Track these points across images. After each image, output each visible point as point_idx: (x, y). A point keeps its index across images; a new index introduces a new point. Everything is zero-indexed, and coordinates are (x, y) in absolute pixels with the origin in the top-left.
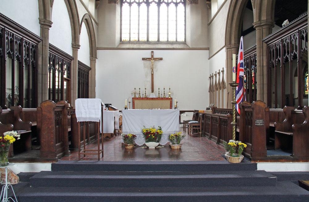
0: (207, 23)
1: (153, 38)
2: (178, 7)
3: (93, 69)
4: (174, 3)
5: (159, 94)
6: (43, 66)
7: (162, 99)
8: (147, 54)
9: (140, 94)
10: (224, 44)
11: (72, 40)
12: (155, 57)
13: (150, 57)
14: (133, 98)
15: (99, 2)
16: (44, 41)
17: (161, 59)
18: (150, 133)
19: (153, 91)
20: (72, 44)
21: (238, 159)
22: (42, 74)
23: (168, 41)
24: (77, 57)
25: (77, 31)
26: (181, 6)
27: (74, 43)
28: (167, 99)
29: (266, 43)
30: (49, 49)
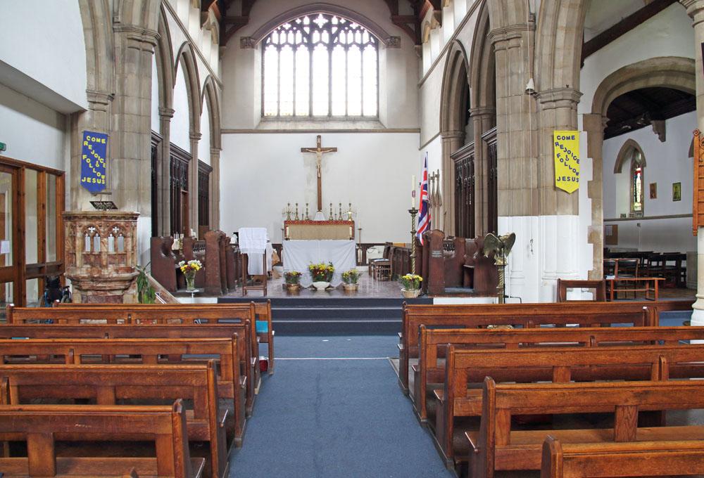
0: (417, 84)
1: (320, 111)
2: (364, 51)
3: (215, 169)
4: (358, 45)
5: (331, 213)
6: (164, 177)
7: (337, 223)
8: (310, 141)
9: (297, 213)
10: (438, 131)
11: (190, 125)
12: (324, 145)
13: (315, 146)
14: (285, 222)
15: (225, 47)
16: (164, 141)
17: (335, 150)
18: (318, 270)
19: (320, 208)
20: (190, 133)
21: (414, 293)
22: (162, 190)
23: (346, 115)
24: (196, 154)
25: (169, 81)
26: (370, 50)
27: (192, 130)
28: (346, 223)
29: (487, 140)
30: (170, 151)
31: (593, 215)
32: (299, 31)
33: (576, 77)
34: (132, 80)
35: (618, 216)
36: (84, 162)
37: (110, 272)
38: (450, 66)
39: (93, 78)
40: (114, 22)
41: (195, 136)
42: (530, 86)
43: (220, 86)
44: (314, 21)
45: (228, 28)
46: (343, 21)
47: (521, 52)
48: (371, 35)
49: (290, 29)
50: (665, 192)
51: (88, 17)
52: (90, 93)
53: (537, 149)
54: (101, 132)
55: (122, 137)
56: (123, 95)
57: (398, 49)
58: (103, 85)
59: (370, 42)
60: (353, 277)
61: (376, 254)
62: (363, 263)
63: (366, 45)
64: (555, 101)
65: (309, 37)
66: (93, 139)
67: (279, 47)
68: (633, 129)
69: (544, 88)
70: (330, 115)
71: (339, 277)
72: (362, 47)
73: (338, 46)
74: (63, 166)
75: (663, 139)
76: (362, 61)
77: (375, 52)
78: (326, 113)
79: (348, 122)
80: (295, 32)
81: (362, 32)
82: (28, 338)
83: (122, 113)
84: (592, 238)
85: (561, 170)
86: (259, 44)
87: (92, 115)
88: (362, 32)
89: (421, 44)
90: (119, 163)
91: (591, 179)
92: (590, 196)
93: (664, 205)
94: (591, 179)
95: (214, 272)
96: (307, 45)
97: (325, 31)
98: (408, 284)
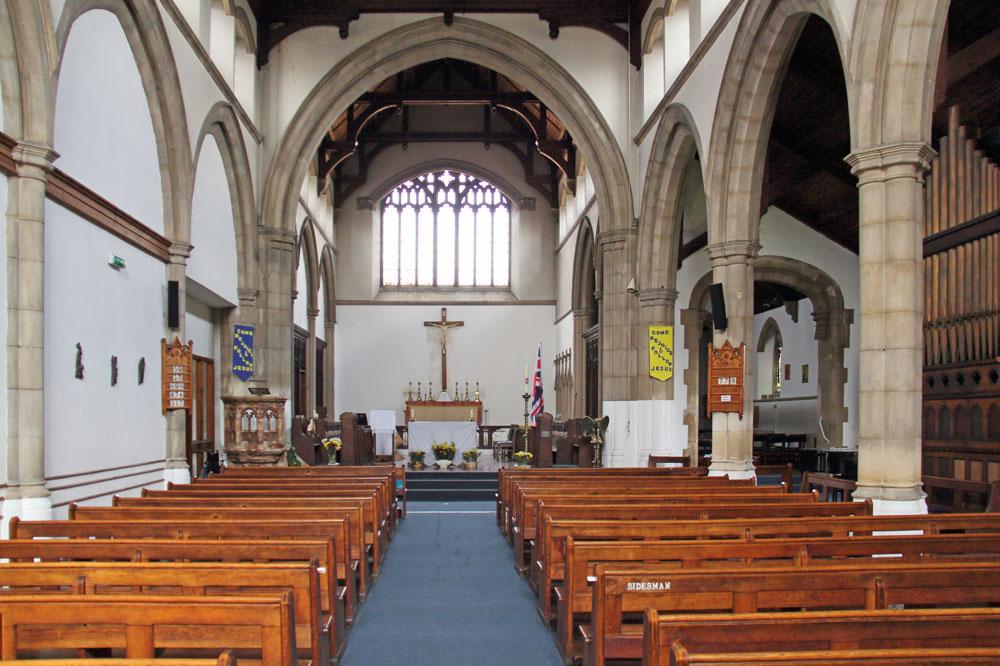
4: (488, 206)
5: (457, 393)
7: (463, 404)
8: (434, 313)
10: (570, 308)
12: (449, 319)
14: (407, 403)
15: (339, 210)
17: (461, 324)
18: (441, 449)
19: (444, 388)
26: (502, 211)
28: (473, 404)
31: (688, 399)
32: (422, 190)
33: (672, 277)
34: (274, 278)
35: (760, 398)
36: (235, 352)
37: (264, 447)
38: (581, 242)
39: (242, 279)
40: (259, 226)
41: (312, 312)
42: (631, 285)
43: (335, 252)
44: (439, 178)
45: (344, 188)
46: (471, 178)
47: (625, 254)
48: (502, 195)
49: (412, 187)
50: (796, 373)
51: (239, 224)
52: (242, 292)
53: (636, 343)
54: (248, 325)
55: (267, 329)
56: (267, 292)
57: (533, 212)
58: (251, 283)
59: (502, 203)
60: (473, 456)
61: (501, 437)
62: (489, 447)
63: (497, 206)
64: (652, 300)
65: (434, 196)
66: (243, 332)
67: (400, 208)
68: (772, 307)
69: (643, 288)
70: (456, 284)
71: (461, 456)
72: (493, 208)
73: (466, 207)
74: (213, 353)
75: (795, 319)
76: (492, 223)
77: (507, 214)
78: (452, 283)
79: (476, 293)
80: (417, 191)
81: (493, 191)
82: (94, 538)
83: (266, 307)
84: (687, 420)
85: (655, 361)
86: (377, 205)
87: (241, 309)
88: (493, 191)
89: (558, 207)
90: (264, 352)
91: (687, 368)
92: (686, 382)
93: (793, 388)
94: (687, 368)
95: (351, 449)
96: (430, 205)
97: (451, 190)
98: (521, 460)
